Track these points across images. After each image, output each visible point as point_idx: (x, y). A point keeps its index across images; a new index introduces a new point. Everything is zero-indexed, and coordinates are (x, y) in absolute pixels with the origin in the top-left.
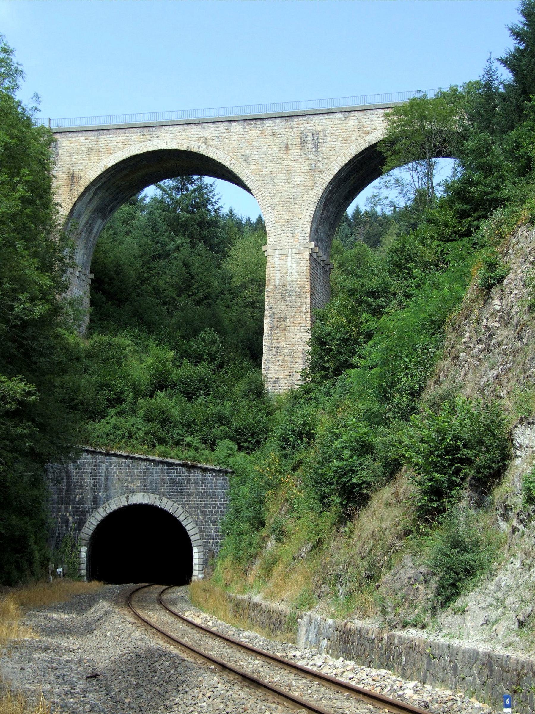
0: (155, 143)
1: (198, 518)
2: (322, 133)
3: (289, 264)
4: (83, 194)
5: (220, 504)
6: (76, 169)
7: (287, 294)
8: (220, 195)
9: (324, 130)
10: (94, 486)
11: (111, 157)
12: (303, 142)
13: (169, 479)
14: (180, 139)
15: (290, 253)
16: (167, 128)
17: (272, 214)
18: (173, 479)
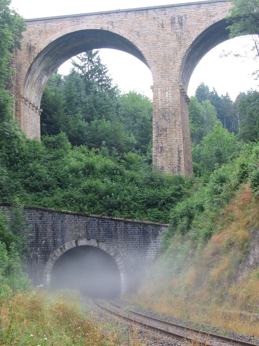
0: (81, 26)
1: (123, 254)
2: (184, 17)
3: (167, 96)
4: (37, 58)
5: (137, 245)
6: (32, 44)
7: (166, 114)
8: (106, 70)
9: (185, 15)
10: (54, 234)
11: (54, 35)
12: (173, 22)
13: (103, 229)
14: (96, 23)
15: (167, 89)
16: (88, 17)
17: (155, 66)
18: (106, 229)
